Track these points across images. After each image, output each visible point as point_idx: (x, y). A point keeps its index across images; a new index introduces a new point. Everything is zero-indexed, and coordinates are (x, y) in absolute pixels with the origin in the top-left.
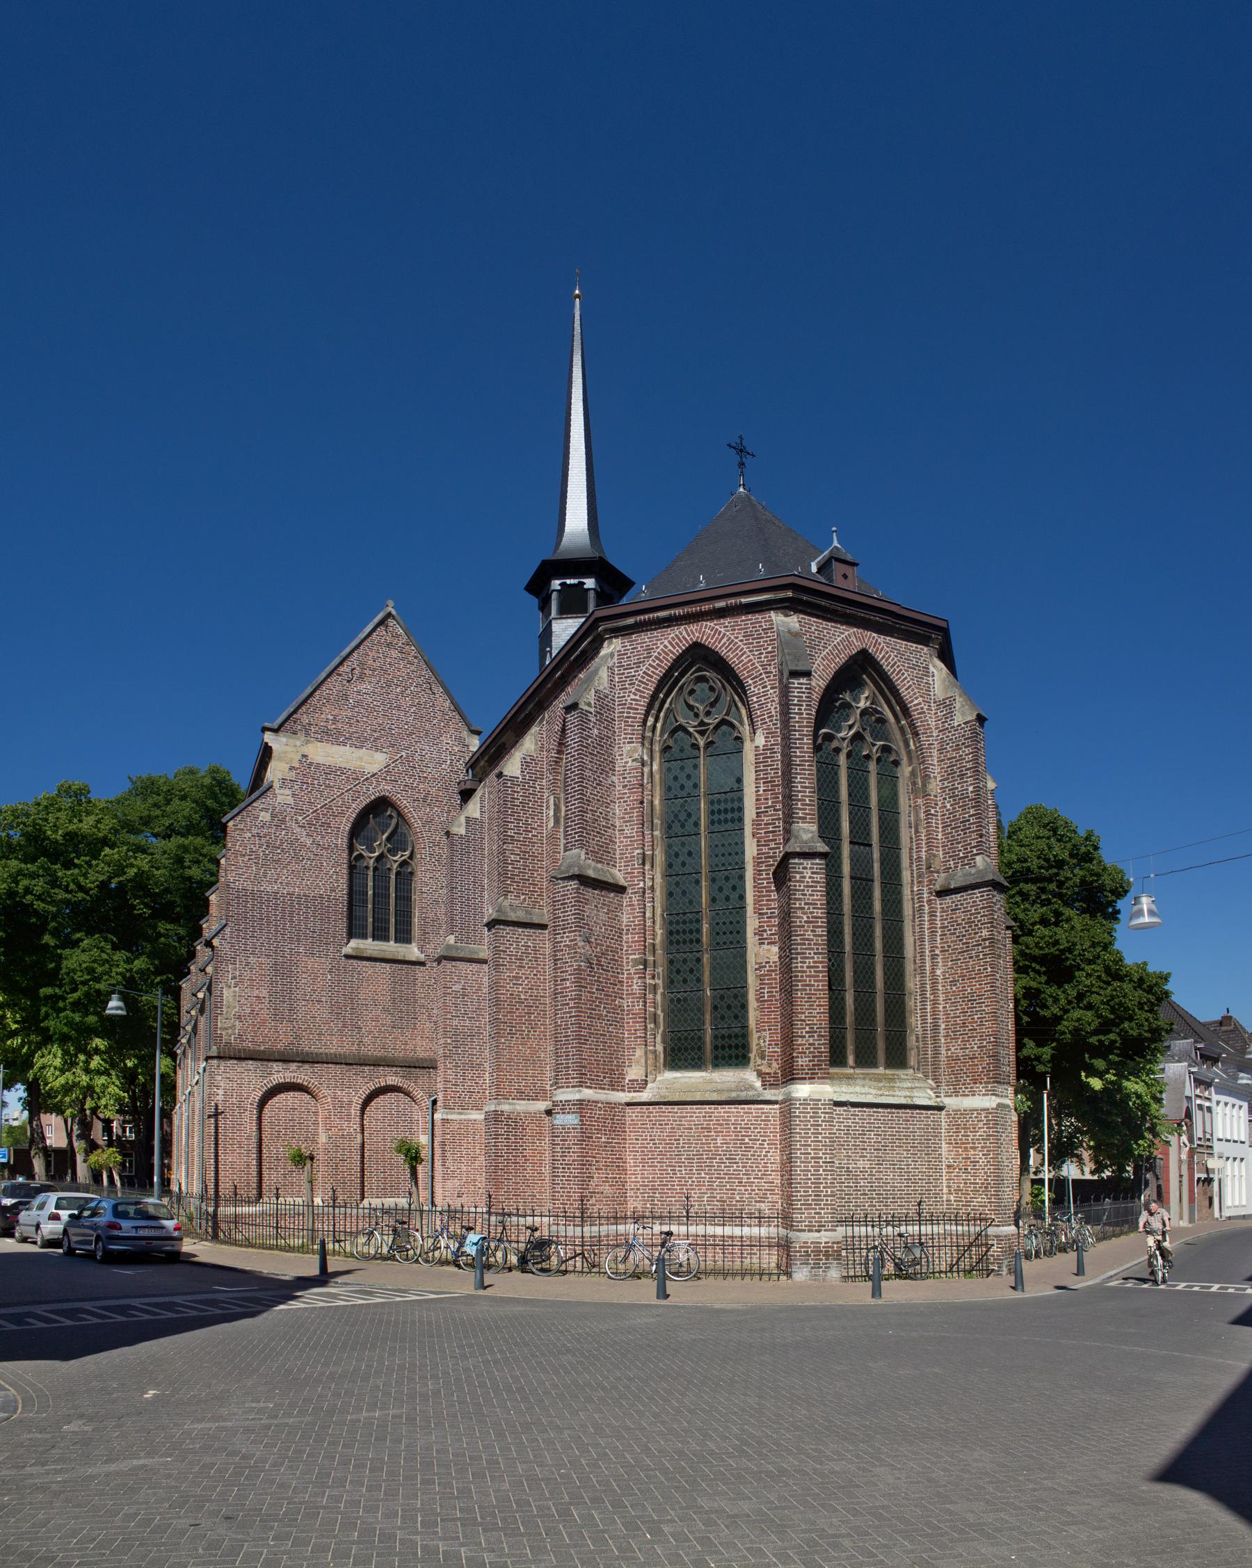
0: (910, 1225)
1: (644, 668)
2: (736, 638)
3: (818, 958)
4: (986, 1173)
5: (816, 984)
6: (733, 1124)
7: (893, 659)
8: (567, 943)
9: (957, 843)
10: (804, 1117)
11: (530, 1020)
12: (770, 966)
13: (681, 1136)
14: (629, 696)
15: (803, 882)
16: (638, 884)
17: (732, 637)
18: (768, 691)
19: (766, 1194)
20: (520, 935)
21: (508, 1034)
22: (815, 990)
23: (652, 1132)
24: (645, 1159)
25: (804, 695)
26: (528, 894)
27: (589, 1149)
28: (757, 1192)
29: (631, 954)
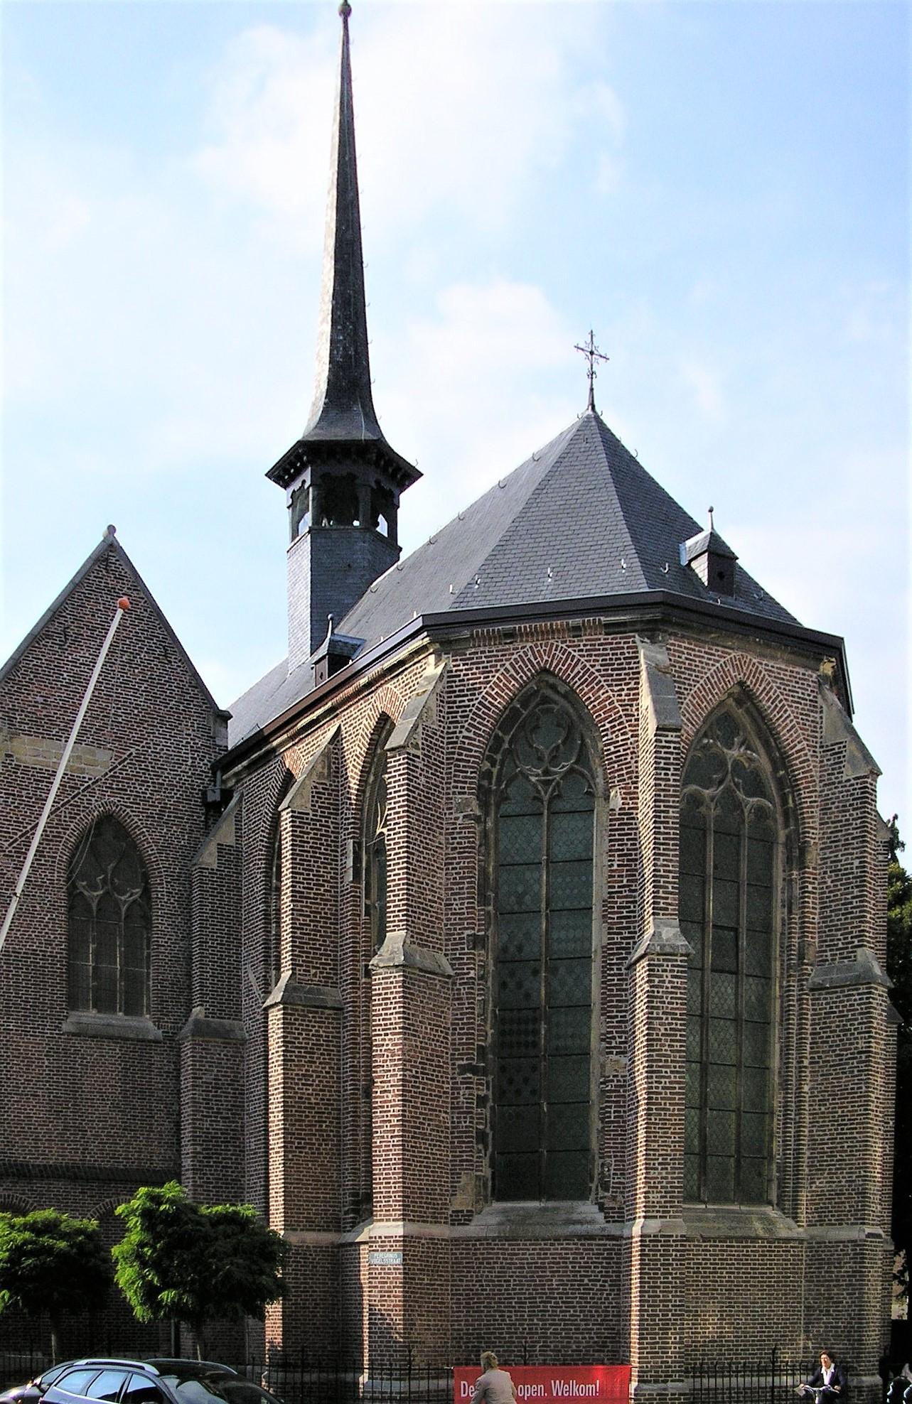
0: (762, 1376)
1: (480, 697)
2: (593, 666)
3: (675, 1077)
4: (849, 1315)
5: (672, 1108)
6: (571, 1263)
7: (776, 691)
8: (390, 1047)
9: (837, 930)
10: (653, 1255)
11: (321, 1131)
12: (618, 1081)
13: (512, 1276)
14: (461, 732)
15: (662, 987)
16: (468, 973)
17: (588, 664)
18: (628, 739)
19: (606, 1342)
20: (310, 1021)
21: (296, 1148)
22: (670, 1115)
23: (479, 1272)
24: (469, 1303)
25: (672, 757)
26: (318, 968)
27: (412, 1292)
28: (596, 1340)
29: (457, 1059)
